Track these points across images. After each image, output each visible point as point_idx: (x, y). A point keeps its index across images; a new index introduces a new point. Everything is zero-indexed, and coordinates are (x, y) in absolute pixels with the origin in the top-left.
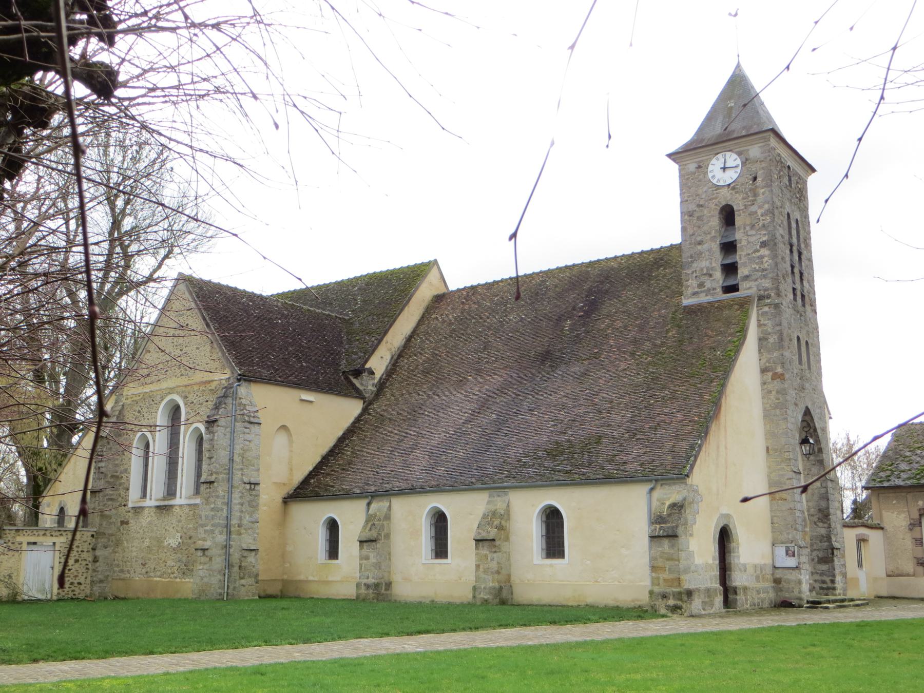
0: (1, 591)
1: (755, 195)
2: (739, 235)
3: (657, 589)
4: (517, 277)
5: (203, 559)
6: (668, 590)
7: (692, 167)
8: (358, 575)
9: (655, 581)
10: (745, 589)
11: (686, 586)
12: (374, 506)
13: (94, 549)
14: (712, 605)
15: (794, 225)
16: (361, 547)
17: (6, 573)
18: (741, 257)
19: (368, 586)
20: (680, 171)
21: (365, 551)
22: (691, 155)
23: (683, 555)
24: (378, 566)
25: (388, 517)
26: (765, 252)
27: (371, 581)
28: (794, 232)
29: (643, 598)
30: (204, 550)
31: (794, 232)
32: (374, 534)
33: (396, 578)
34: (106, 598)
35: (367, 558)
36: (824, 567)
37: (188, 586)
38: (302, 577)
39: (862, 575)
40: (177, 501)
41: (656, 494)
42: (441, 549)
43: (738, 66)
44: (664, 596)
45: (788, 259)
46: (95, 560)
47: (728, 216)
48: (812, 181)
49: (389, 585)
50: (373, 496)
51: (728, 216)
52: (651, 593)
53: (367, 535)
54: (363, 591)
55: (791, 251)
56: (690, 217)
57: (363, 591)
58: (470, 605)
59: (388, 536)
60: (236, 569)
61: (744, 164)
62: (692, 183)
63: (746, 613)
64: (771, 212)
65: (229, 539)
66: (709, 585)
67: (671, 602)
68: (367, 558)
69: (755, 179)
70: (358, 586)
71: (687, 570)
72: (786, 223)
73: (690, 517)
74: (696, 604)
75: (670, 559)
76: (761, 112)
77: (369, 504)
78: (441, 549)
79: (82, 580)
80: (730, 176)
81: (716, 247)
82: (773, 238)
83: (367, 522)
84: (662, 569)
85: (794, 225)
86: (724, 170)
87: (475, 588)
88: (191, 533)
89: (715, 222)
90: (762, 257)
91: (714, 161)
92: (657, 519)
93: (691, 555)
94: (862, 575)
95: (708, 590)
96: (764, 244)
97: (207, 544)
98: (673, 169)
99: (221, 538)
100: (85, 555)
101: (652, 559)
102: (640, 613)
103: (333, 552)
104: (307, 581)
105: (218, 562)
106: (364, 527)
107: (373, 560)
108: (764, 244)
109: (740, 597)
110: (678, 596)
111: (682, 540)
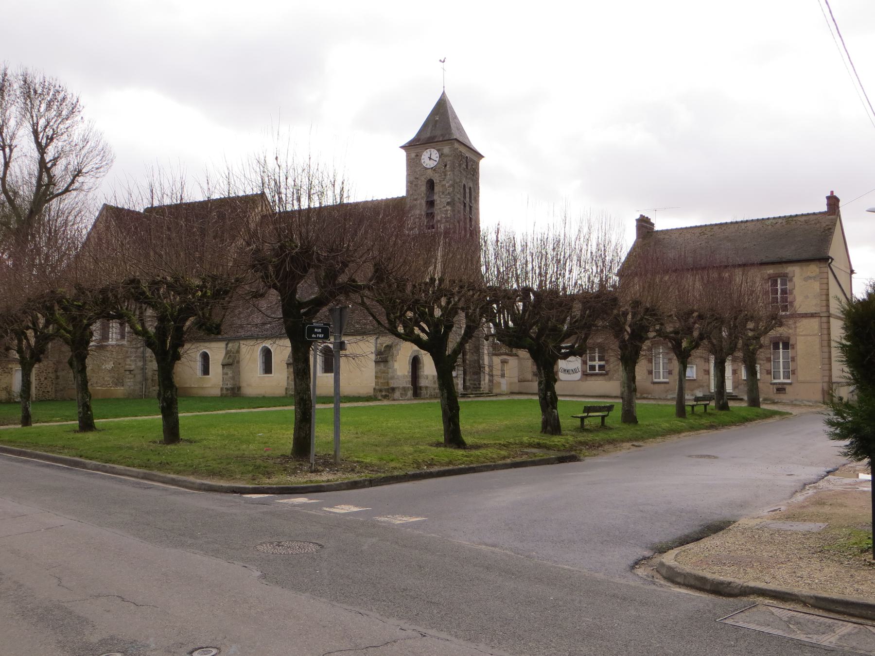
0: (3, 396)
1: (445, 175)
2: (436, 197)
3: (377, 387)
4: (320, 207)
5: (130, 376)
6: (383, 387)
7: (413, 155)
8: (221, 383)
9: (377, 383)
10: (426, 387)
11: (392, 386)
12: (230, 345)
13: (56, 371)
14: (406, 395)
15: (467, 191)
16: (223, 368)
17: (4, 386)
18: (437, 209)
19: (227, 389)
20: (407, 156)
21: (226, 370)
22: (414, 148)
23: (390, 370)
24: (233, 378)
25: (238, 352)
26: (449, 208)
27: (229, 386)
28: (468, 195)
29: (370, 392)
30: (130, 371)
31: (468, 195)
32: (231, 361)
33: (243, 384)
34: (65, 400)
35: (227, 374)
36: (476, 377)
37: (120, 391)
38: (188, 385)
39: (503, 381)
40: (111, 342)
41: (379, 341)
42: (268, 369)
43: (444, 93)
44: (381, 391)
45: (462, 211)
46: (57, 377)
47: (431, 184)
48: (482, 163)
49: (239, 388)
50: (228, 340)
51: (431, 184)
52: (374, 389)
53: (227, 361)
54: (225, 392)
55: (465, 206)
56: (411, 184)
57: (225, 392)
58: (283, 397)
59: (238, 362)
60: (150, 381)
61: (440, 157)
62: (413, 164)
63: (424, 399)
64: (453, 186)
65: (145, 364)
66: (405, 385)
67: (384, 393)
68: (227, 374)
69: (446, 166)
70: (222, 389)
71: (392, 378)
72: (462, 191)
73: (395, 352)
74: (397, 394)
75: (384, 372)
76: (453, 125)
77: (227, 345)
78: (268, 369)
79: (50, 390)
80: (431, 164)
81: (424, 202)
82: (453, 200)
83: (226, 354)
84: (380, 378)
85: (467, 191)
86: (430, 158)
87: (286, 389)
88: (120, 361)
89: (424, 188)
90: (447, 210)
91: (425, 153)
92: (379, 353)
93: (395, 370)
94: (503, 381)
95: (404, 389)
96: (448, 204)
97: (133, 367)
98: (403, 154)
99: (140, 364)
100: (50, 375)
101: (376, 373)
102: (368, 399)
103: (206, 371)
104: (191, 388)
105: (139, 378)
106: (225, 357)
107: (230, 375)
108: (448, 204)
109: (424, 392)
110: (387, 390)
111: (390, 363)
